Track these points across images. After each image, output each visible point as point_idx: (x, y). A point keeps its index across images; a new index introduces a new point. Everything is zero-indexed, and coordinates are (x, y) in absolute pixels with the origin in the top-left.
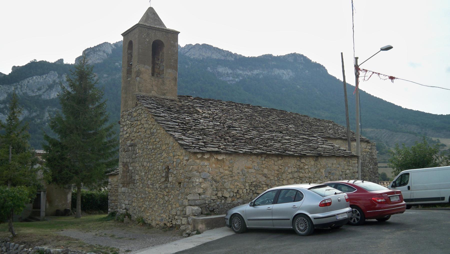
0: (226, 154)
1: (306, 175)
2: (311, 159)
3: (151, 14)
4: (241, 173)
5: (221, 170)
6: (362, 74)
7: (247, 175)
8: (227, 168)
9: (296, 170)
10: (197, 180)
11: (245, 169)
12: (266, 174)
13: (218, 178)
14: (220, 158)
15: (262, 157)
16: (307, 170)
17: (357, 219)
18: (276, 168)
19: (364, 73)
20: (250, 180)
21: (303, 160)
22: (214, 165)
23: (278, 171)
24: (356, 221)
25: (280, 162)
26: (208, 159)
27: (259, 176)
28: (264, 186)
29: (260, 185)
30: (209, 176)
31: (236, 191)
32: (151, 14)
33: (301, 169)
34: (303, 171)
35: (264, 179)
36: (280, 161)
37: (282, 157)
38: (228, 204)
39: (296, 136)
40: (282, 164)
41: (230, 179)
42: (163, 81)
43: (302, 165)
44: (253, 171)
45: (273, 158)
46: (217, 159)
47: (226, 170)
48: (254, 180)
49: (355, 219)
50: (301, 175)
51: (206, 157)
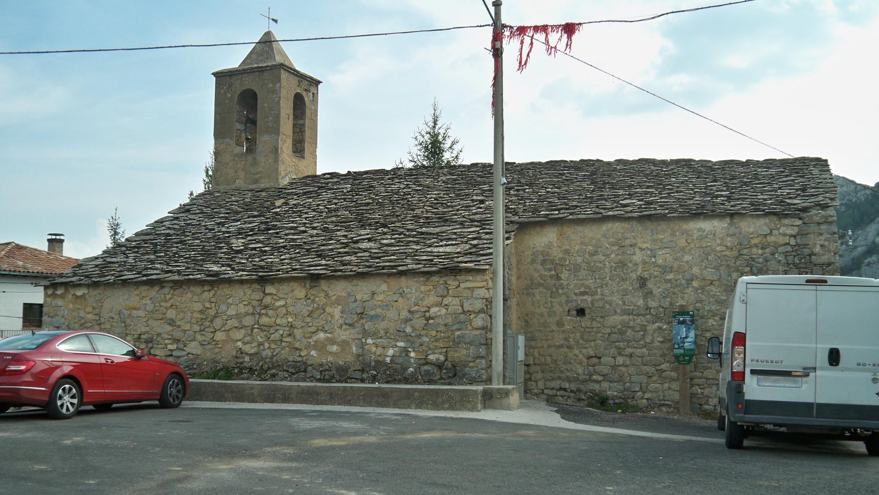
0: (88, 286)
1: (278, 321)
2: (295, 285)
4: (116, 317)
5: (82, 314)
6: (511, 47)
7: (128, 321)
8: (90, 309)
9: (251, 311)
11: (125, 311)
12: (172, 320)
14: (79, 293)
15: (162, 287)
17: (72, 404)
18: (198, 307)
19: (543, 35)
20: (136, 330)
21: (269, 289)
22: (71, 306)
24: (71, 409)
25: (206, 295)
26: (62, 296)
28: (167, 341)
29: (159, 339)
30: (64, 323)
33: (266, 307)
34: (270, 312)
35: (169, 328)
36: (206, 293)
37: (211, 286)
39: (703, 207)
40: (213, 300)
41: (582, 274)
42: (255, 159)
43: (268, 300)
44: (141, 313)
45: (192, 288)
46: (74, 294)
47: (89, 313)
49: (69, 404)
50: (264, 320)
51: (59, 292)
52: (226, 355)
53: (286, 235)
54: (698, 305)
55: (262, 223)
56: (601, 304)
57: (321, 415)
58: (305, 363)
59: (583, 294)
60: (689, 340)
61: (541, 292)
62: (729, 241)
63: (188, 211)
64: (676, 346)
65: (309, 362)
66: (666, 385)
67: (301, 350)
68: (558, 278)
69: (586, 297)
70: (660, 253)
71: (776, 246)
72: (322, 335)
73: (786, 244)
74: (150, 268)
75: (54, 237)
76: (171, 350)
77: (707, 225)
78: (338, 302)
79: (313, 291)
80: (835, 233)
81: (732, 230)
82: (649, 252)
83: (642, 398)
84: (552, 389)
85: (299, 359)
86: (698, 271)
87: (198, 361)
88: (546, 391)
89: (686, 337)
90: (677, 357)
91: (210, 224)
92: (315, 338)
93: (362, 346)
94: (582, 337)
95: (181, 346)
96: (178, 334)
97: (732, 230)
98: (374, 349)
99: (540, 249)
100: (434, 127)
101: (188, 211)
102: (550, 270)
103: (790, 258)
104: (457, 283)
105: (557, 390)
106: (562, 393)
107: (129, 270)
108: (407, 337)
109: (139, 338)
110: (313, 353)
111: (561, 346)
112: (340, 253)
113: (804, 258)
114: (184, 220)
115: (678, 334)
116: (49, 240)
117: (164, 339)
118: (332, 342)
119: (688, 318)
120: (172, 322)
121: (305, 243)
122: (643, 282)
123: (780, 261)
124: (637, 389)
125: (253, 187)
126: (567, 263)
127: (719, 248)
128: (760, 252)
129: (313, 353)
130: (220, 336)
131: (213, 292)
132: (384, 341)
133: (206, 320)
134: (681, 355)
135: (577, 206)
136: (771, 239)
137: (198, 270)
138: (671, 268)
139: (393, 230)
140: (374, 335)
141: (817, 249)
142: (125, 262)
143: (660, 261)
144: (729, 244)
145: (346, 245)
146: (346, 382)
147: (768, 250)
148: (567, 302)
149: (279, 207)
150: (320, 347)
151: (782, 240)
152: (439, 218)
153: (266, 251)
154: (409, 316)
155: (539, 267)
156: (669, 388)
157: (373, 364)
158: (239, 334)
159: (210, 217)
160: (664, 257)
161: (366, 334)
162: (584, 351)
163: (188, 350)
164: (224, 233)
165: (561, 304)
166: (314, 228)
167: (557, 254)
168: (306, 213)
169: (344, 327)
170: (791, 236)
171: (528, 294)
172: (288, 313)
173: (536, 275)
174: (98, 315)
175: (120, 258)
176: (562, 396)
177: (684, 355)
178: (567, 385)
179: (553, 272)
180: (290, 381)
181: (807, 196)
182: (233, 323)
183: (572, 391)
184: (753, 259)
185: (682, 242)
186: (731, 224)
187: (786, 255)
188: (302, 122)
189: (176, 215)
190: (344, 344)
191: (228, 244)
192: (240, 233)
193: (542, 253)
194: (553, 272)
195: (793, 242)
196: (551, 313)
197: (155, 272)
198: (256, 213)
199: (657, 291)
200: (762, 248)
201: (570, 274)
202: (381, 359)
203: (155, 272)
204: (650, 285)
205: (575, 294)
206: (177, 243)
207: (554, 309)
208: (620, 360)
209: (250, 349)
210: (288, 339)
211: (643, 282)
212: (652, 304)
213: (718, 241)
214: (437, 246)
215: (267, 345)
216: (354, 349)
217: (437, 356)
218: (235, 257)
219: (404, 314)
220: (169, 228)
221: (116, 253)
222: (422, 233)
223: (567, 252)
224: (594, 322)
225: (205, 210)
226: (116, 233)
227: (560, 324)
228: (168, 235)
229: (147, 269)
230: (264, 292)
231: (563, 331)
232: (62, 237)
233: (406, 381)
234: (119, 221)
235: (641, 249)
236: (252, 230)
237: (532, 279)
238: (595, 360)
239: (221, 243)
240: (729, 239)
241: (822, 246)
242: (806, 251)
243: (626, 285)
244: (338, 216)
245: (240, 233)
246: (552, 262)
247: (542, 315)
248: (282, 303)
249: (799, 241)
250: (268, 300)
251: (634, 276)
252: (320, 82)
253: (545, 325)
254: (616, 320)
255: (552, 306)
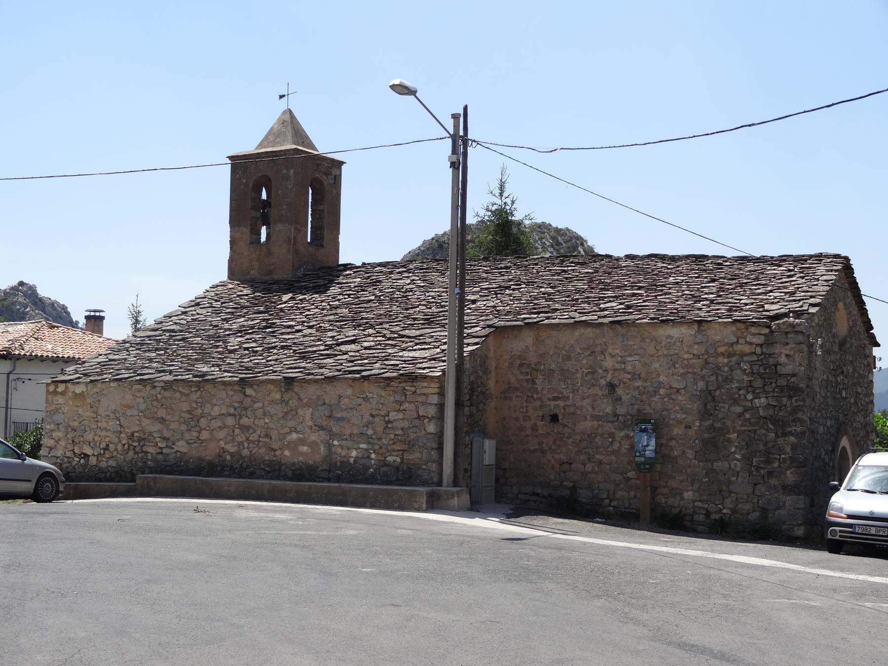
3: (290, 123)
4: (112, 416)
5: (80, 411)
10: (48, 427)
13: (76, 424)
16: (259, 413)
18: (185, 407)
23: (189, 412)
27: (146, 422)
31: (103, 445)
32: (290, 123)
38: (91, 467)
48: (136, 429)
50: (245, 421)
52: (210, 453)
53: (282, 334)
54: (665, 413)
55: (264, 320)
56: (572, 410)
58: (279, 463)
59: (555, 399)
60: (650, 448)
61: (518, 396)
62: (696, 349)
63: (198, 304)
64: (638, 454)
65: (283, 462)
66: (632, 494)
67: (276, 450)
68: (534, 383)
69: (558, 402)
70: (630, 359)
71: (743, 355)
72: (294, 436)
73: (752, 353)
74: (147, 367)
75: (92, 314)
76: (161, 448)
77: (675, 332)
78: (308, 405)
80: (801, 343)
81: (700, 338)
82: (619, 359)
83: (609, 505)
84: (526, 494)
85: (274, 459)
86: (665, 379)
87: (185, 459)
88: (520, 496)
89: (647, 446)
90: (638, 465)
91: (216, 320)
92: (288, 438)
93: (329, 446)
94: (554, 443)
95: (170, 444)
96: (167, 434)
97: (700, 338)
98: (340, 450)
99: (518, 354)
100: (501, 195)
101: (198, 304)
102: (527, 374)
103: (755, 368)
104: (413, 389)
105: (531, 495)
106: (535, 498)
107: (127, 369)
108: (368, 439)
109: (133, 435)
110: (287, 453)
111: (535, 451)
112: (322, 355)
113: (770, 368)
114: (192, 315)
115: (639, 442)
116: (86, 317)
117: (155, 438)
118: (302, 442)
119: (649, 427)
120: (162, 420)
121: (294, 343)
122: (612, 387)
123: (745, 370)
124: (605, 496)
125: (267, 278)
126: (542, 367)
127: (686, 356)
128: (726, 360)
129: (287, 453)
130: (205, 435)
131: (199, 393)
132: (349, 443)
133: (193, 420)
134: (642, 463)
135: (557, 310)
136: (738, 348)
137: (189, 370)
138: (639, 375)
139: (378, 332)
140: (340, 437)
141: (783, 359)
142: (125, 359)
143: (629, 368)
144: (696, 352)
145: (330, 347)
146: (315, 481)
147: (734, 359)
148: (541, 407)
149: (285, 303)
150: (293, 446)
151: (747, 349)
152: (426, 320)
153: (257, 351)
154: (371, 419)
155: (516, 372)
156: (635, 496)
157: (338, 464)
158: (221, 434)
161: (332, 435)
162: (556, 456)
163: (176, 448)
164: (226, 330)
165: (535, 409)
166: (310, 327)
167: (532, 358)
168: (309, 310)
169: (314, 428)
170: (757, 345)
171: (506, 398)
172: (265, 415)
173: (513, 380)
174: (96, 413)
176: (535, 502)
177: (645, 463)
178: (539, 491)
179: (529, 377)
180: (267, 479)
181: (795, 301)
182: (217, 423)
183: (544, 497)
184: (719, 368)
185: (651, 349)
186: (699, 331)
187: (752, 363)
188: (321, 207)
189: (184, 310)
190: (313, 445)
191: (225, 342)
193: (519, 357)
194: (529, 377)
195: (758, 350)
196: (527, 418)
197: (150, 371)
198: (262, 309)
199: (625, 398)
200: (728, 357)
201: (544, 379)
202: (345, 460)
203: (150, 371)
204: (619, 391)
205: (549, 399)
206: (180, 340)
207: (528, 414)
208: (589, 467)
209: (232, 449)
210: (266, 440)
211: (612, 387)
212: (621, 410)
213: (686, 349)
214: (410, 350)
215: (246, 445)
216: (322, 449)
217: (394, 458)
218: (227, 357)
219: (367, 418)
220: (176, 323)
221: (119, 350)
222: (403, 336)
223: (542, 356)
224: (566, 428)
225: (215, 304)
226: (137, 321)
227: (534, 428)
228: (173, 331)
229: (143, 368)
230: (244, 394)
231: (537, 436)
232: (102, 314)
233: (366, 481)
234: (140, 309)
235: (613, 356)
236: (252, 328)
237: (509, 383)
238: (566, 467)
239: (219, 341)
240: (696, 347)
241: (787, 356)
242: (772, 361)
243: (597, 391)
244: (336, 314)
245: (241, 331)
246: (529, 366)
247: (517, 419)
248: (260, 405)
249: (764, 350)
251: (604, 383)
252: (342, 163)
253: (521, 429)
254: (587, 425)
255: (527, 411)
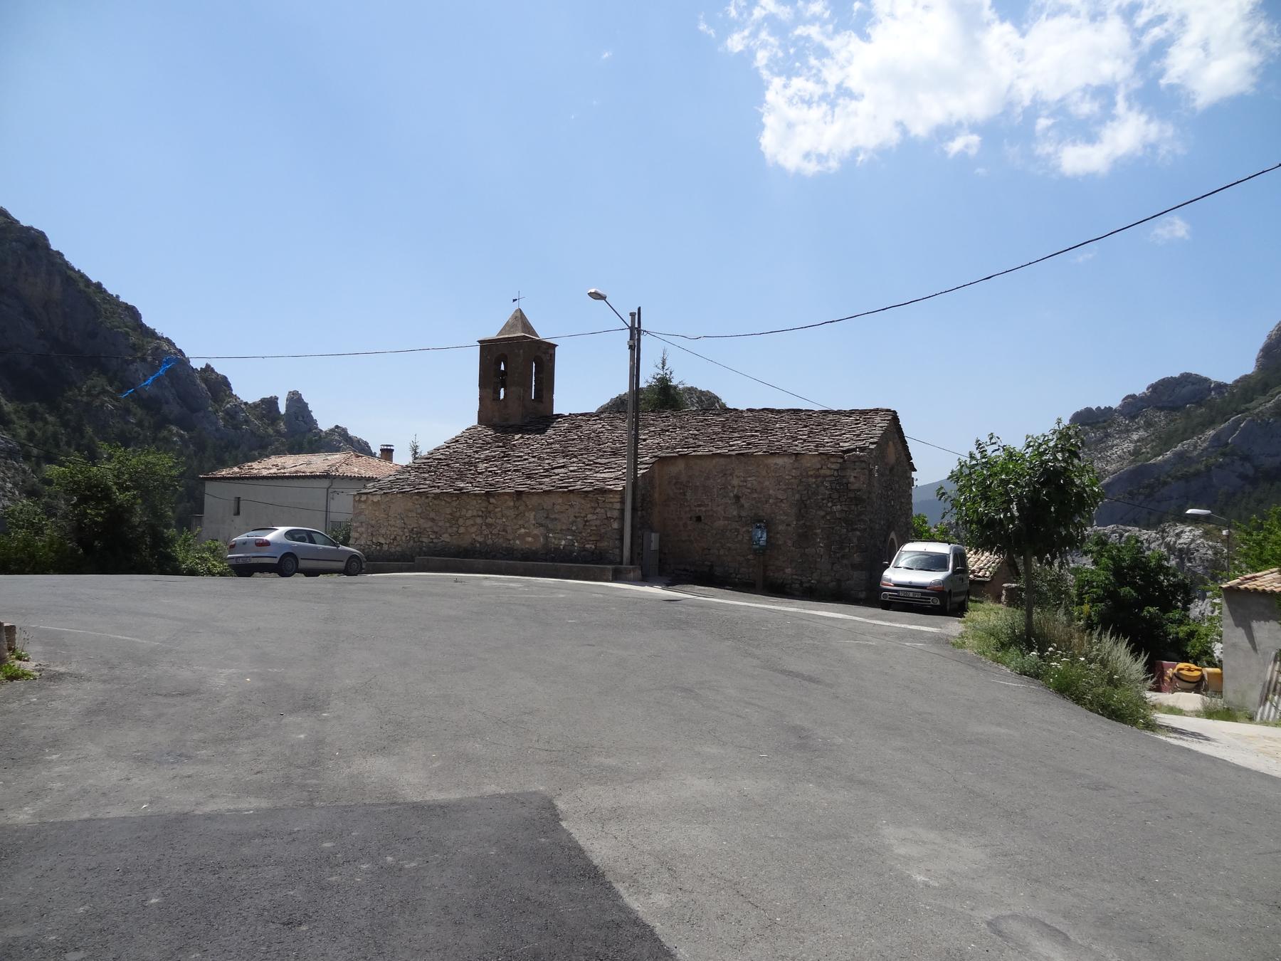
18: (448, 511)
21: (492, 500)
43: (491, 507)
52: (465, 542)
57: (497, 580)
62: (794, 473)
71: (825, 476)
72: (523, 530)
79: (518, 504)
81: (796, 465)
91: (470, 452)
93: (547, 538)
96: (436, 529)
97: (796, 465)
108: (573, 533)
118: (528, 535)
120: (433, 520)
122: (737, 498)
130: (462, 530)
133: (454, 519)
136: (822, 472)
141: (852, 479)
145: (547, 470)
150: (522, 537)
151: (828, 472)
158: (473, 529)
159: (470, 447)
160: (752, 480)
175: (406, 476)
182: (469, 522)
187: (831, 482)
190: (535, 537)
192: (487, 459)
199: (746, 505)
204: (743, 501)
208: (722, 552)
209: (480, 539)
212: (743, 514)
227: (685, 525)
245: (487, 459)
250: (491, 507)
